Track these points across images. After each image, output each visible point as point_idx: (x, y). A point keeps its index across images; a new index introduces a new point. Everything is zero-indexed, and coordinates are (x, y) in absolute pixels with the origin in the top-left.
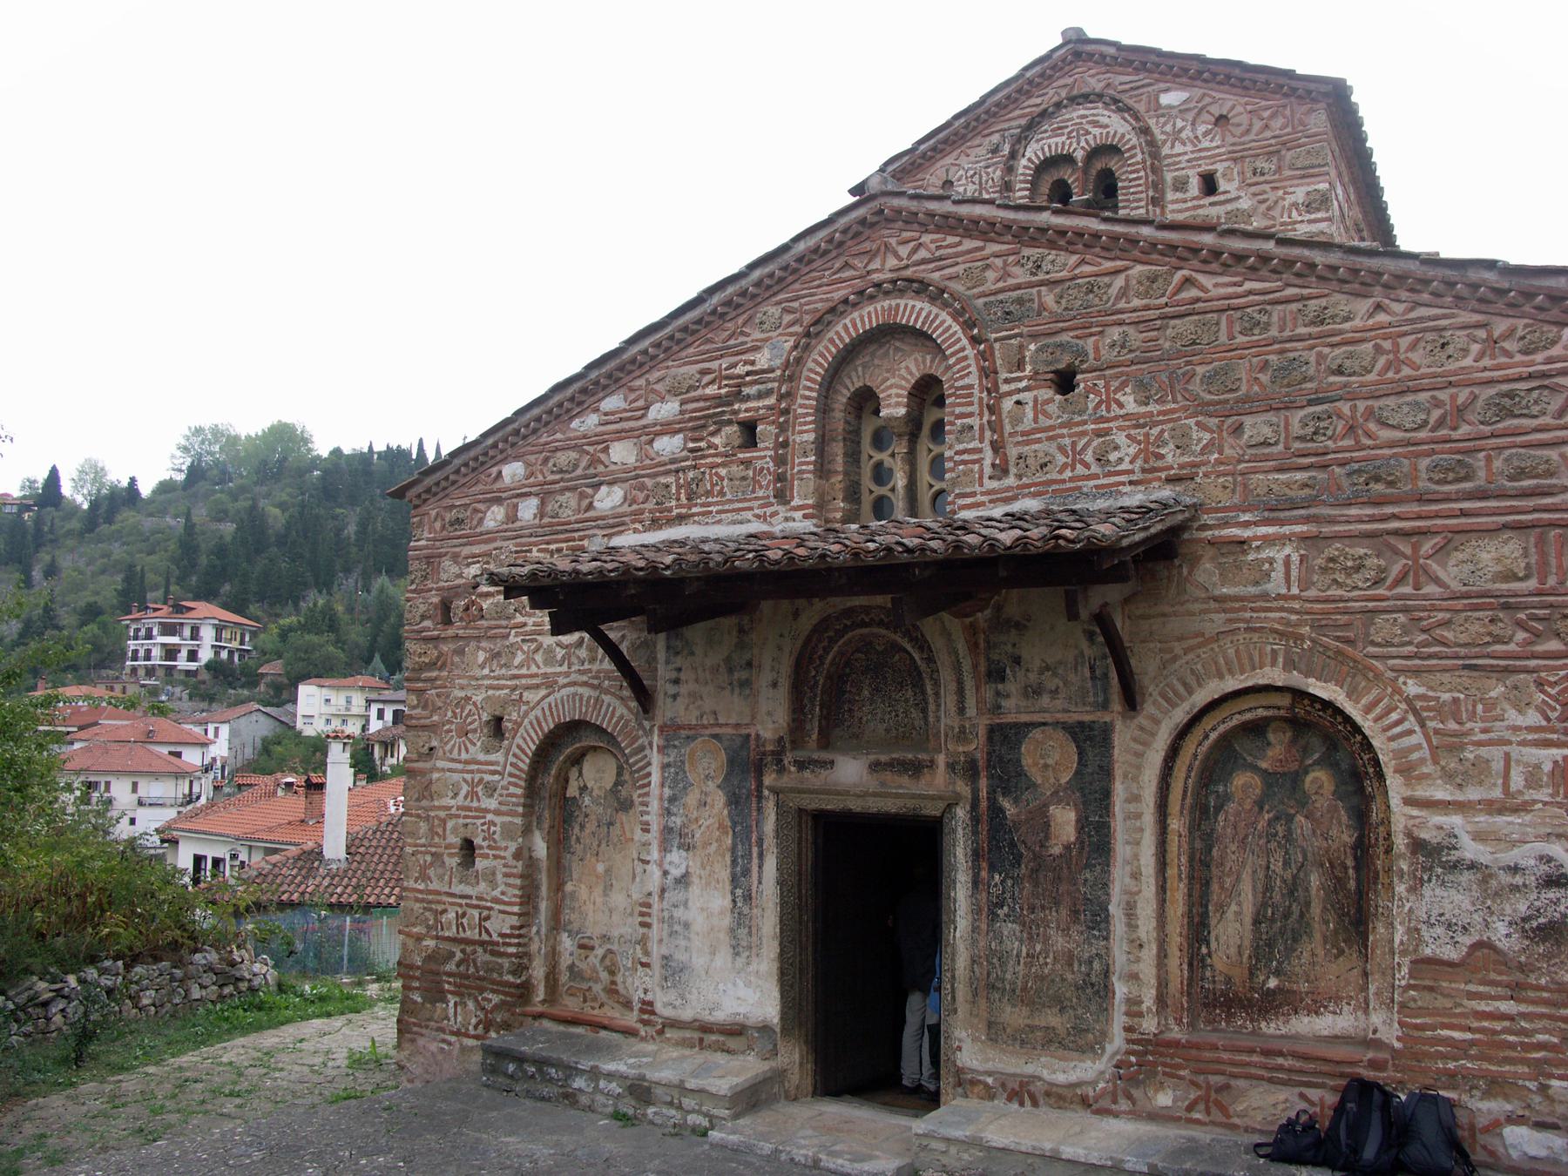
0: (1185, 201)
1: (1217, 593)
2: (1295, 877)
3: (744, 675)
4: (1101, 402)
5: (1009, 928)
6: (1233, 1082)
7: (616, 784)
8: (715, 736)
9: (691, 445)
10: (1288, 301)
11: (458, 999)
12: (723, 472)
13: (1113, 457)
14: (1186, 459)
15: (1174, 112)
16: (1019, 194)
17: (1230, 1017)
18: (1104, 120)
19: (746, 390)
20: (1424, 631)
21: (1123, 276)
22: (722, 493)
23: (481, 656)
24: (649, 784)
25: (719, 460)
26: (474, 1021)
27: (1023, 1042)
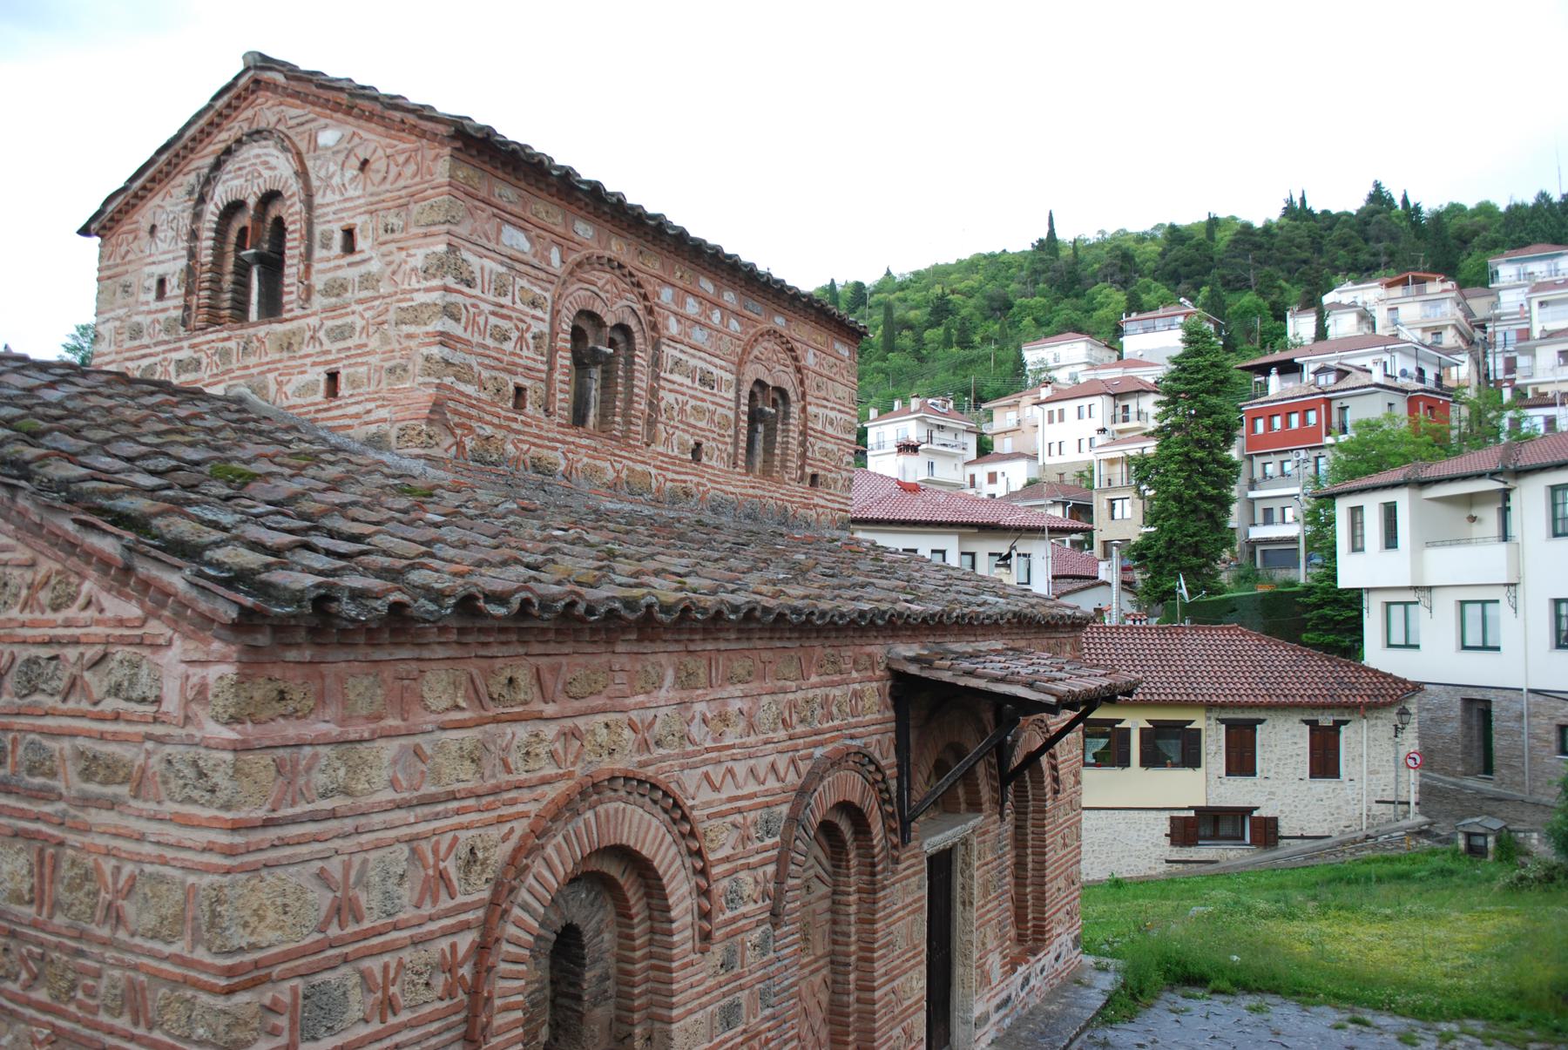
0: (328, 260)
18: (273, 161)
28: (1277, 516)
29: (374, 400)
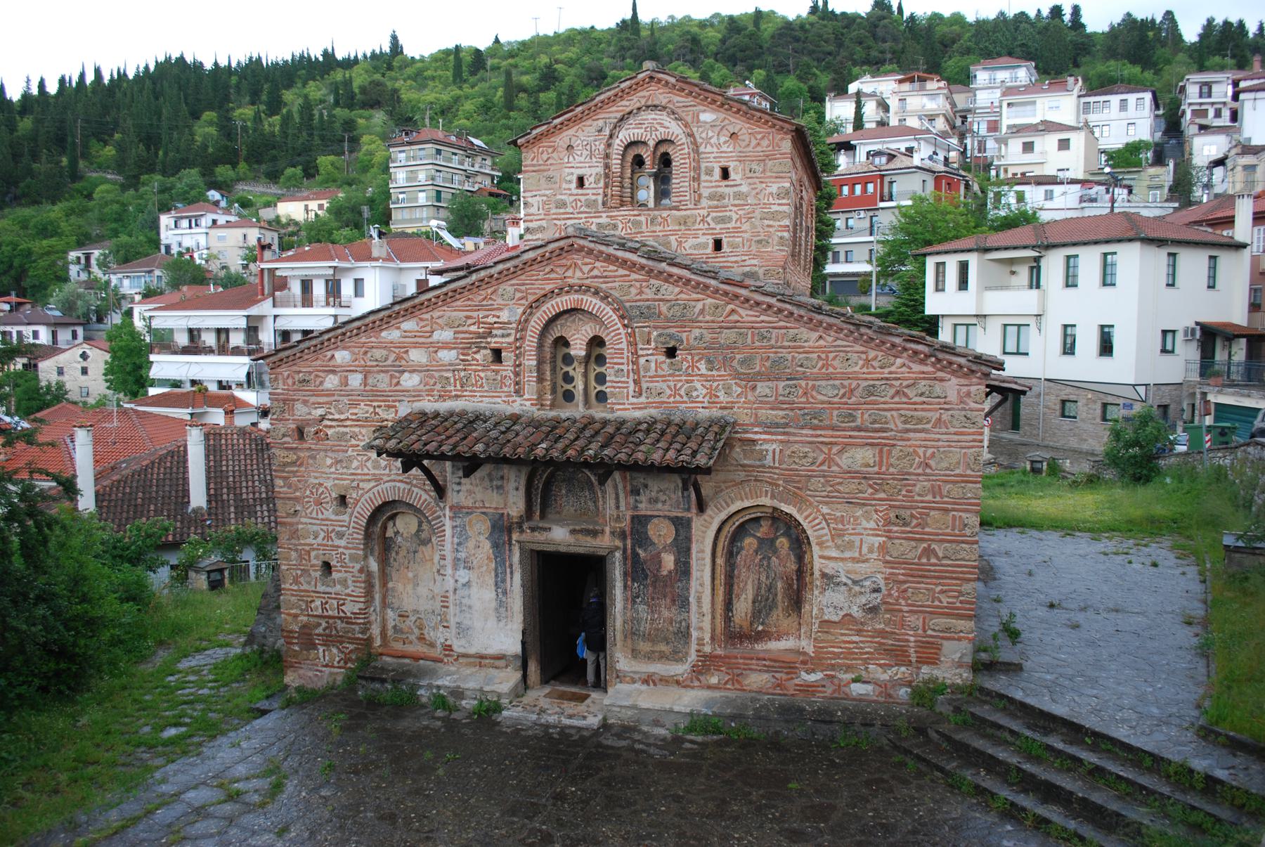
4: (689, 367)
5: (641, 608)
7: (418, 531)
8: (483, 513)
9: (462, 357)
12: (482, 375)
13: (695, 394)
14: (729, 399)
16: (614, 162)
17: (741, 643)
18: (667, 124)
21: (701, 303)
22: (482, 386)
25: (480, 368)
26: (337, 659)
28: (842, 257)
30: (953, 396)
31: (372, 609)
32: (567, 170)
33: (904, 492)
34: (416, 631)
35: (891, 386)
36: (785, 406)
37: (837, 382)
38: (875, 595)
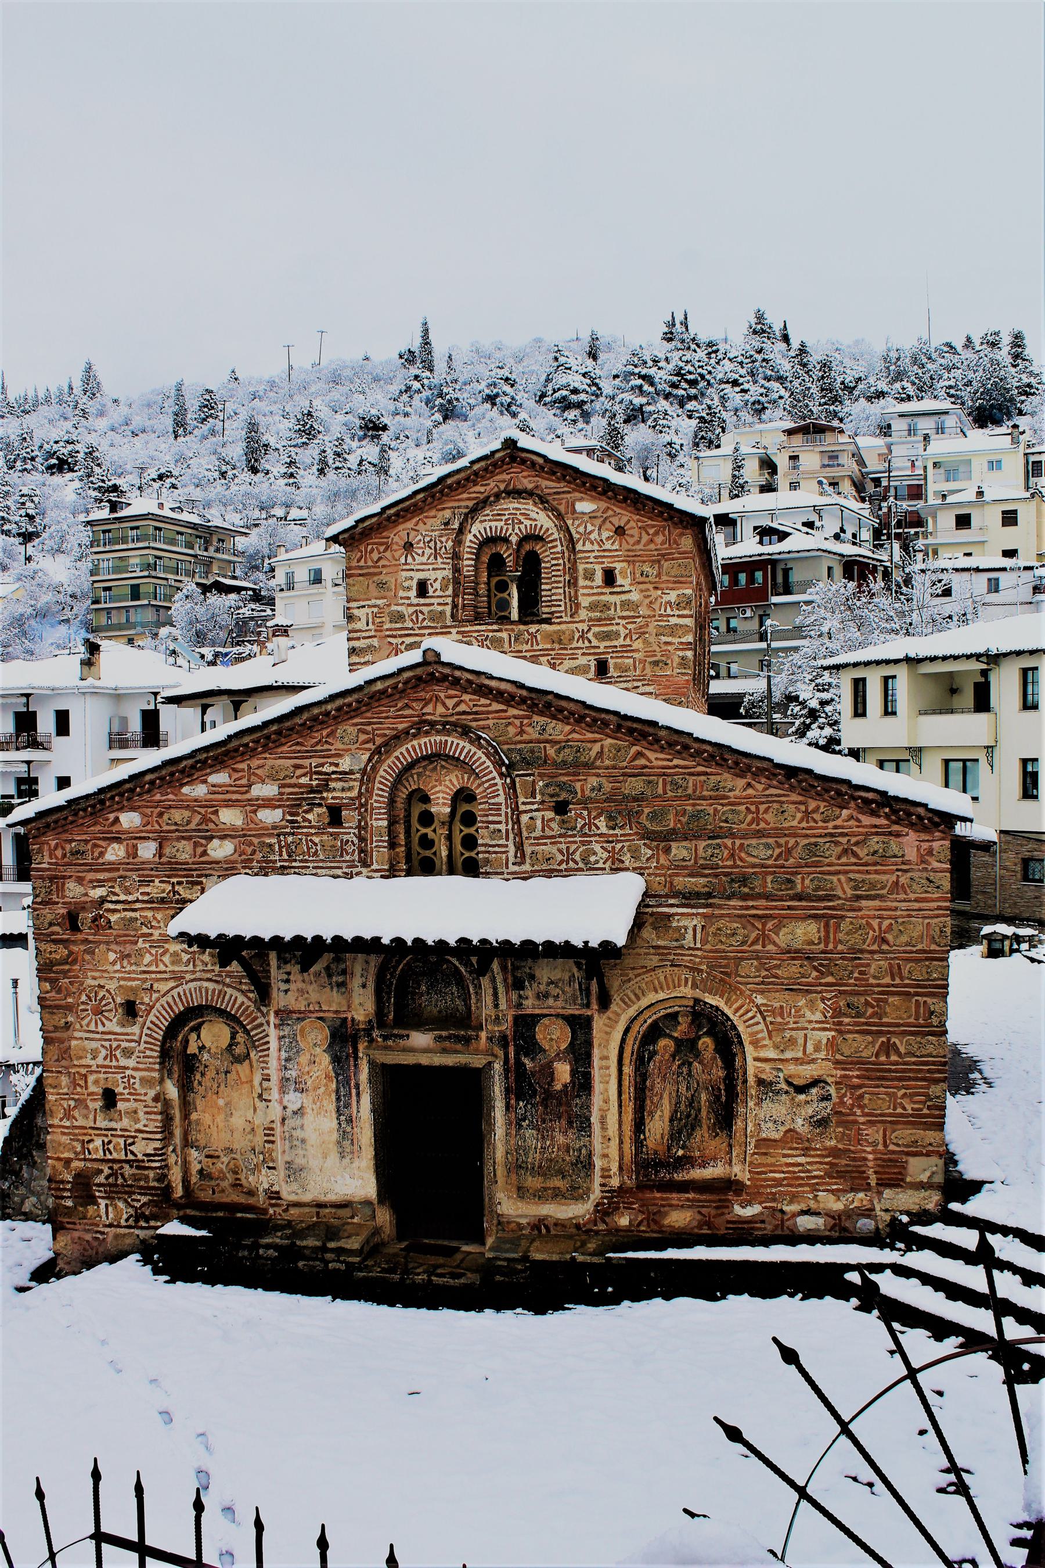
0: (592, 588)
1: (654, 944)
2: (693, 1096)
3: (340, 979)
4: (585, 824)
5: (529, 1133)
6: (662, 1209)
7: (230, 1045)
9: (289, 818)
10: (699, 774)
11: (108, 1202)
12: (316, 840)
13: (593, 859)
15: (586, 518)
16: (466, 563)
18: (533, 515)
19: (332, 785)
20: (766, 970)
21: (599, 744)
22: (316, 853)
23: (112, 956)
24: (268, 1049)
25: (313, 831)
26: (125, 1216)
27: (540, 1197)
29: (640, 680)
30: (911, 855)
31: (171, 1148)
32: (404, 574)
33: (856, 975)
34: (230, 1177)
35: (837, 843)
36: (707, 872)
37: (771, 841)
38: (823, 1104)
